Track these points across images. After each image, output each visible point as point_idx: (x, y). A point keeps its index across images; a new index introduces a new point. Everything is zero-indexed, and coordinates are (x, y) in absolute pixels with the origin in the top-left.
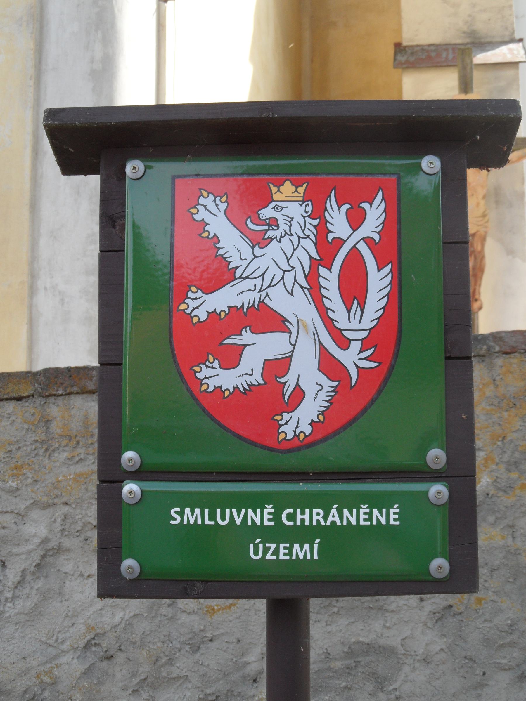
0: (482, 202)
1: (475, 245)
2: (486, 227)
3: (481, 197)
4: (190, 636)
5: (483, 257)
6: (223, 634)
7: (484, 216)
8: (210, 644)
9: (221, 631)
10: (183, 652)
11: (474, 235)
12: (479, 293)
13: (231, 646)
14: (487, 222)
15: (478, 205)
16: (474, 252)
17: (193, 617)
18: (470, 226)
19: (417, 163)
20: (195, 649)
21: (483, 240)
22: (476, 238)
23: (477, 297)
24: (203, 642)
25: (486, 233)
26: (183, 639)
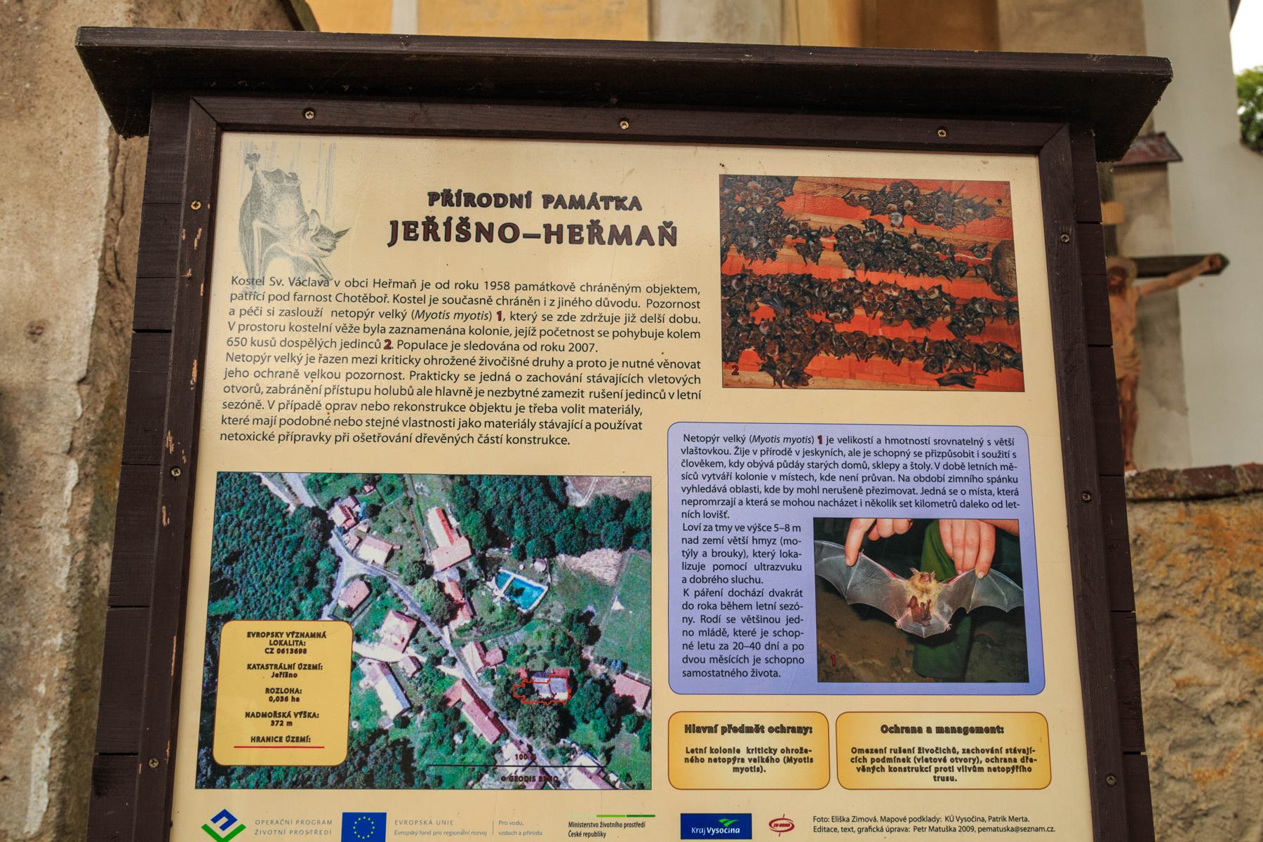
0: (1130, 339)
1: (1123, 393)
2: (1137, 370)
3: (1128, 331)
4: (1181, 809)
5: (1134, 409)
6: (1218, 807)
7: (1133, 355)
8: (1204, 820)
9: (1217, 803)
10: (1175, 828)
11: (1121, 380)
12: (1131, 455)
13: (1228, 823)
14: (1139, 363)
15: (1125, 342)
16: (1122, 402)
17: (1183, 785)
18: (1117, 369)
19: (222, 506)
20: (1188, 824)
21: (1134, 386)
22: (1124, 385)
23: (1128, 459)
24: (1196, 817)
25: (1137, 378)
26: (1173, 813)
